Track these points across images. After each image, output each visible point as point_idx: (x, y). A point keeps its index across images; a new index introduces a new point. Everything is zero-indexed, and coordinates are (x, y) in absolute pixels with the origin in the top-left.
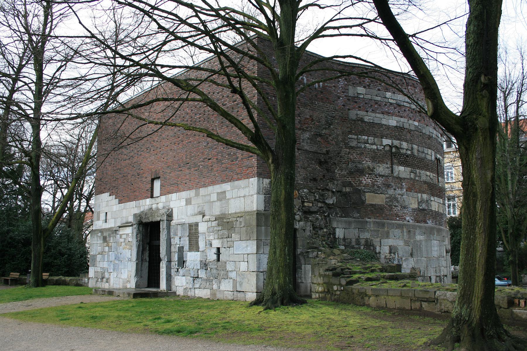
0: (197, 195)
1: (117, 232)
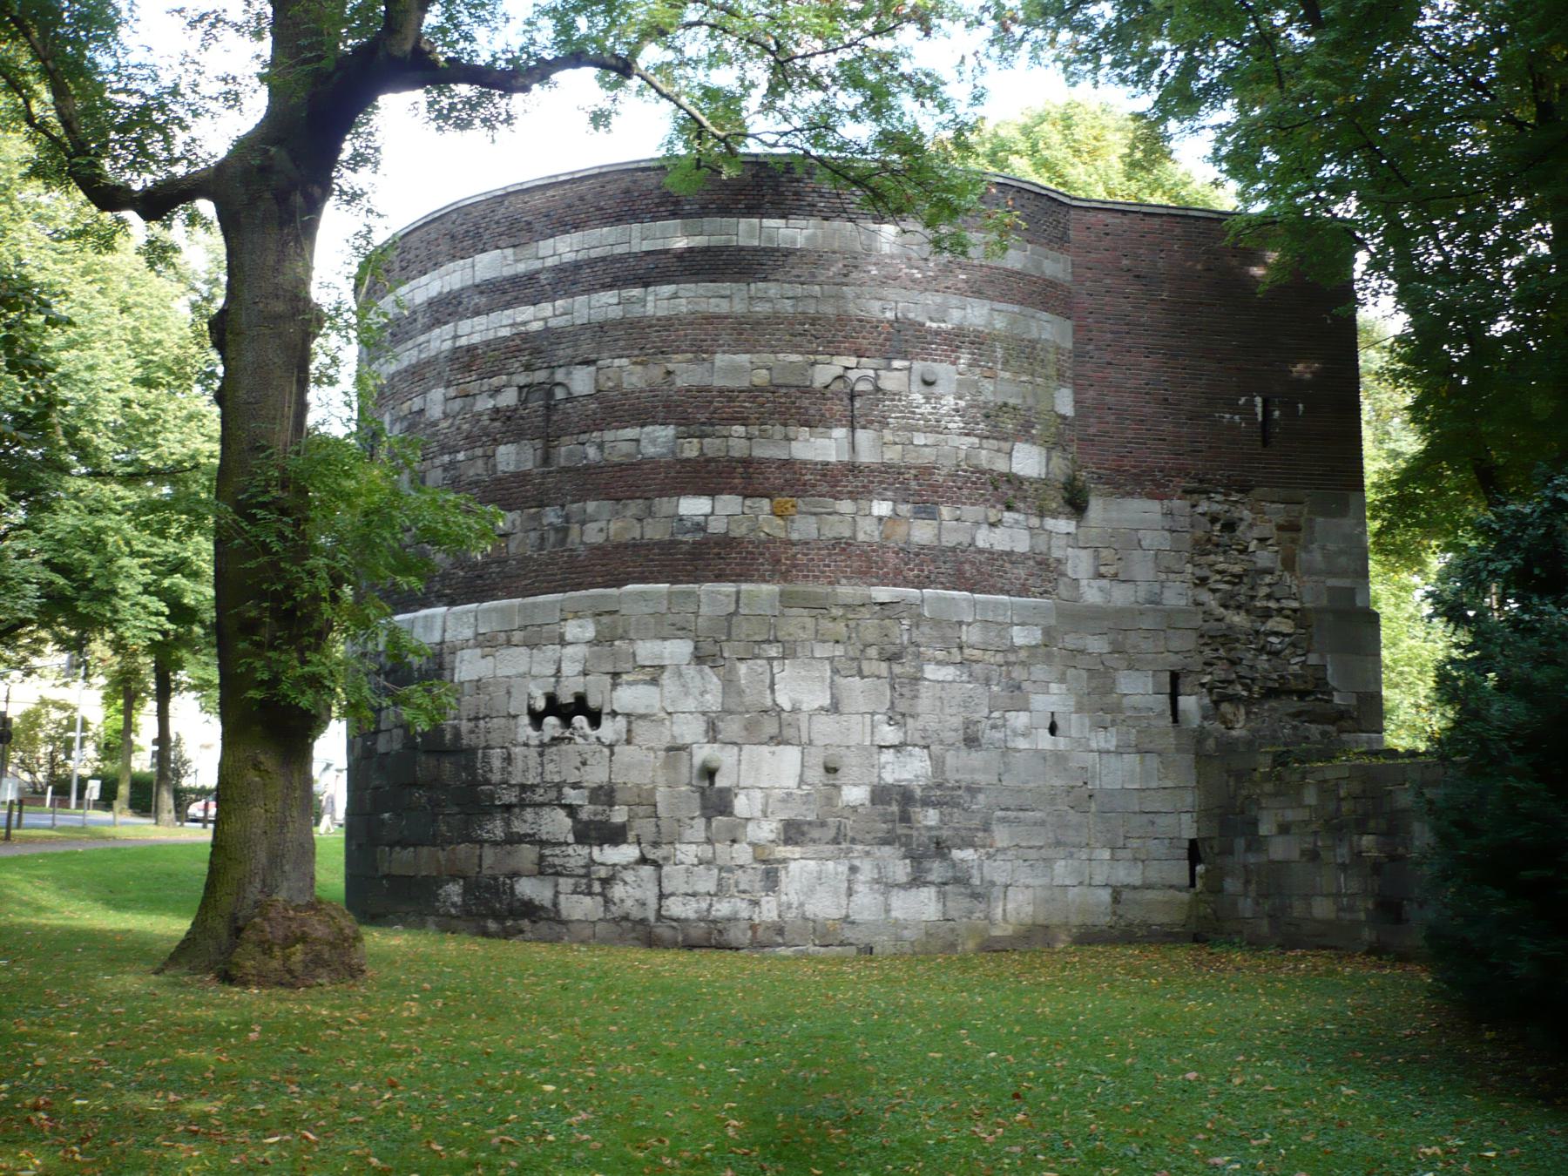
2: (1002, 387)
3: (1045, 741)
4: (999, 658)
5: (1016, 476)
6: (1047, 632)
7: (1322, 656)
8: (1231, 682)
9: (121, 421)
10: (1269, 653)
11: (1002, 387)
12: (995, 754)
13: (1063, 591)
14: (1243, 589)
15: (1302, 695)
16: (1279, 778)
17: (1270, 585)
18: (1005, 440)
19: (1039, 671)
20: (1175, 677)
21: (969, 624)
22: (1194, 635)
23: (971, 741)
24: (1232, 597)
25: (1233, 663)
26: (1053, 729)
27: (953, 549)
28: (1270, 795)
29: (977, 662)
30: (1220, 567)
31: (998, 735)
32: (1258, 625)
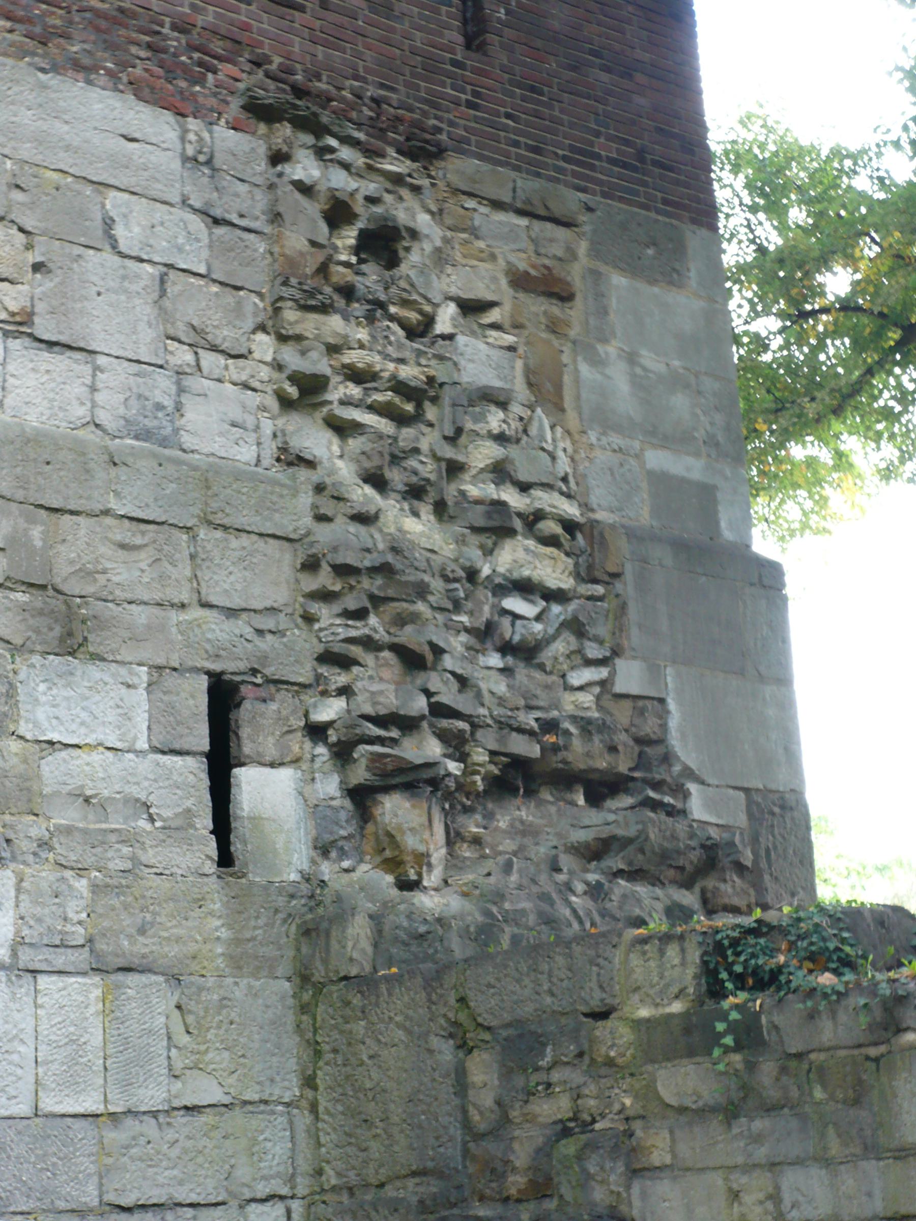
7: (655, 672)
8: (408, 724)
9: (181, 1175)
10: (506, 648)
14: (428, 440)
15: (600, 788)
16: (749, 1036)
17: (501, 438)
20: (223, 697)
22: (286, 560)
24: (395, 460)
25: (413, 661)
28: (692, 1114)
30: (352, 357)
32: (474, 554)
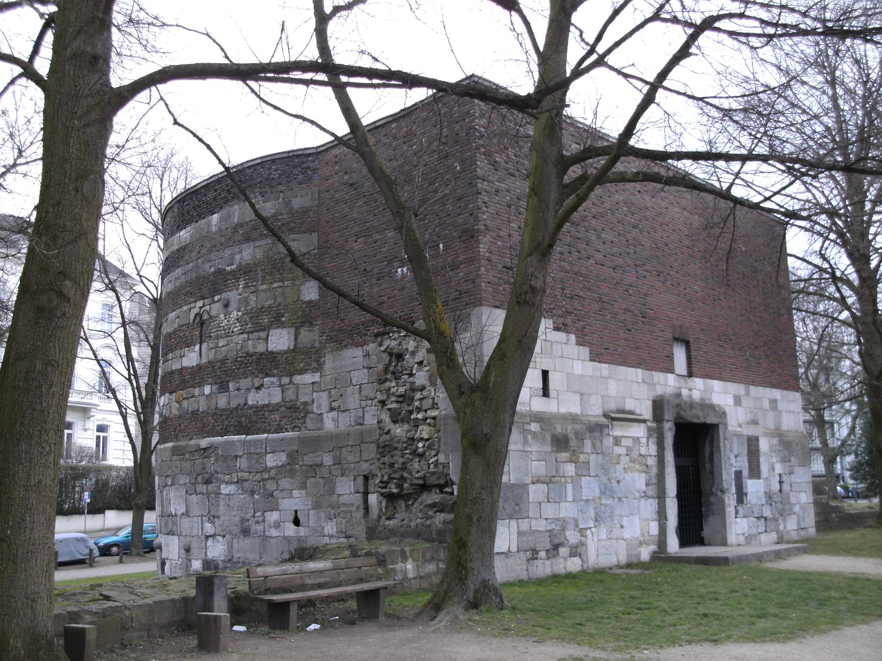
0: (748, 393)
1: (606, 431)
2: (263, 296)
3: (290, 530)
4: (258, 477)
5: (272, 353)
6: (290, 455)
7: (447, 456)
11: (263, 296)
12: (257, 540)
13: (309, 423)
18: (263, 330)
19: (285, 483)
21: (240, 457)
23: (246, 532)
26: (297, 522)
27: (236, 409)
29: (246, 480)
31: (260, 528)
